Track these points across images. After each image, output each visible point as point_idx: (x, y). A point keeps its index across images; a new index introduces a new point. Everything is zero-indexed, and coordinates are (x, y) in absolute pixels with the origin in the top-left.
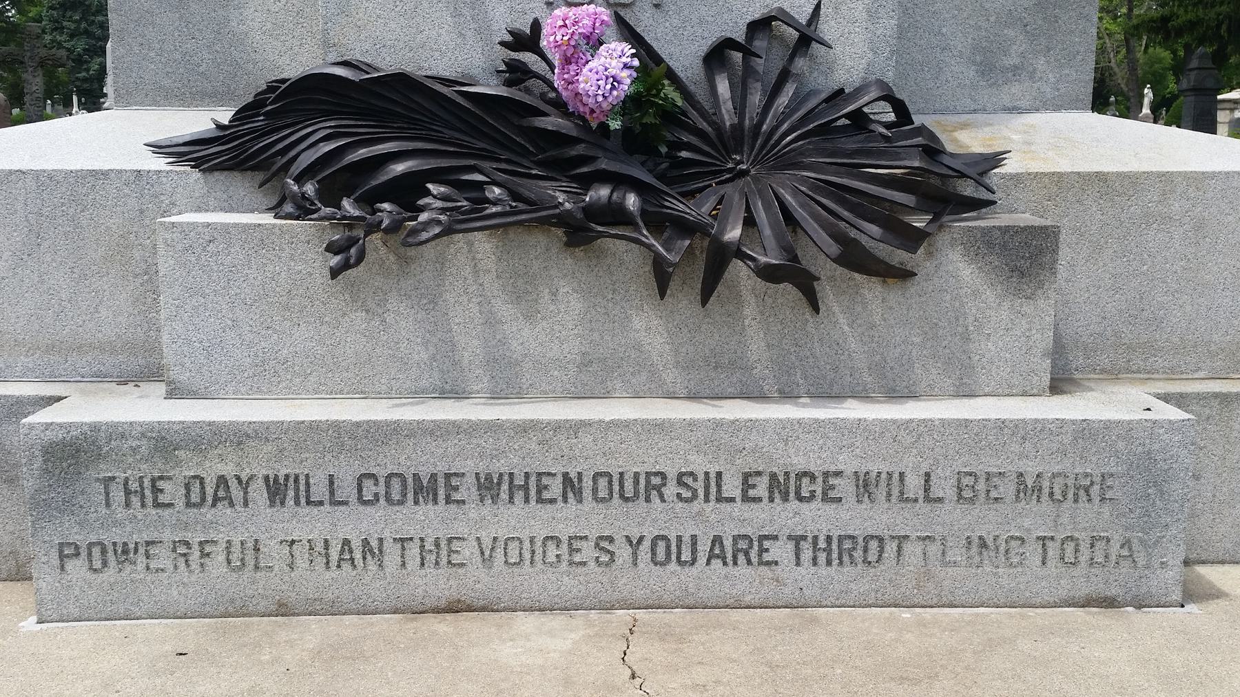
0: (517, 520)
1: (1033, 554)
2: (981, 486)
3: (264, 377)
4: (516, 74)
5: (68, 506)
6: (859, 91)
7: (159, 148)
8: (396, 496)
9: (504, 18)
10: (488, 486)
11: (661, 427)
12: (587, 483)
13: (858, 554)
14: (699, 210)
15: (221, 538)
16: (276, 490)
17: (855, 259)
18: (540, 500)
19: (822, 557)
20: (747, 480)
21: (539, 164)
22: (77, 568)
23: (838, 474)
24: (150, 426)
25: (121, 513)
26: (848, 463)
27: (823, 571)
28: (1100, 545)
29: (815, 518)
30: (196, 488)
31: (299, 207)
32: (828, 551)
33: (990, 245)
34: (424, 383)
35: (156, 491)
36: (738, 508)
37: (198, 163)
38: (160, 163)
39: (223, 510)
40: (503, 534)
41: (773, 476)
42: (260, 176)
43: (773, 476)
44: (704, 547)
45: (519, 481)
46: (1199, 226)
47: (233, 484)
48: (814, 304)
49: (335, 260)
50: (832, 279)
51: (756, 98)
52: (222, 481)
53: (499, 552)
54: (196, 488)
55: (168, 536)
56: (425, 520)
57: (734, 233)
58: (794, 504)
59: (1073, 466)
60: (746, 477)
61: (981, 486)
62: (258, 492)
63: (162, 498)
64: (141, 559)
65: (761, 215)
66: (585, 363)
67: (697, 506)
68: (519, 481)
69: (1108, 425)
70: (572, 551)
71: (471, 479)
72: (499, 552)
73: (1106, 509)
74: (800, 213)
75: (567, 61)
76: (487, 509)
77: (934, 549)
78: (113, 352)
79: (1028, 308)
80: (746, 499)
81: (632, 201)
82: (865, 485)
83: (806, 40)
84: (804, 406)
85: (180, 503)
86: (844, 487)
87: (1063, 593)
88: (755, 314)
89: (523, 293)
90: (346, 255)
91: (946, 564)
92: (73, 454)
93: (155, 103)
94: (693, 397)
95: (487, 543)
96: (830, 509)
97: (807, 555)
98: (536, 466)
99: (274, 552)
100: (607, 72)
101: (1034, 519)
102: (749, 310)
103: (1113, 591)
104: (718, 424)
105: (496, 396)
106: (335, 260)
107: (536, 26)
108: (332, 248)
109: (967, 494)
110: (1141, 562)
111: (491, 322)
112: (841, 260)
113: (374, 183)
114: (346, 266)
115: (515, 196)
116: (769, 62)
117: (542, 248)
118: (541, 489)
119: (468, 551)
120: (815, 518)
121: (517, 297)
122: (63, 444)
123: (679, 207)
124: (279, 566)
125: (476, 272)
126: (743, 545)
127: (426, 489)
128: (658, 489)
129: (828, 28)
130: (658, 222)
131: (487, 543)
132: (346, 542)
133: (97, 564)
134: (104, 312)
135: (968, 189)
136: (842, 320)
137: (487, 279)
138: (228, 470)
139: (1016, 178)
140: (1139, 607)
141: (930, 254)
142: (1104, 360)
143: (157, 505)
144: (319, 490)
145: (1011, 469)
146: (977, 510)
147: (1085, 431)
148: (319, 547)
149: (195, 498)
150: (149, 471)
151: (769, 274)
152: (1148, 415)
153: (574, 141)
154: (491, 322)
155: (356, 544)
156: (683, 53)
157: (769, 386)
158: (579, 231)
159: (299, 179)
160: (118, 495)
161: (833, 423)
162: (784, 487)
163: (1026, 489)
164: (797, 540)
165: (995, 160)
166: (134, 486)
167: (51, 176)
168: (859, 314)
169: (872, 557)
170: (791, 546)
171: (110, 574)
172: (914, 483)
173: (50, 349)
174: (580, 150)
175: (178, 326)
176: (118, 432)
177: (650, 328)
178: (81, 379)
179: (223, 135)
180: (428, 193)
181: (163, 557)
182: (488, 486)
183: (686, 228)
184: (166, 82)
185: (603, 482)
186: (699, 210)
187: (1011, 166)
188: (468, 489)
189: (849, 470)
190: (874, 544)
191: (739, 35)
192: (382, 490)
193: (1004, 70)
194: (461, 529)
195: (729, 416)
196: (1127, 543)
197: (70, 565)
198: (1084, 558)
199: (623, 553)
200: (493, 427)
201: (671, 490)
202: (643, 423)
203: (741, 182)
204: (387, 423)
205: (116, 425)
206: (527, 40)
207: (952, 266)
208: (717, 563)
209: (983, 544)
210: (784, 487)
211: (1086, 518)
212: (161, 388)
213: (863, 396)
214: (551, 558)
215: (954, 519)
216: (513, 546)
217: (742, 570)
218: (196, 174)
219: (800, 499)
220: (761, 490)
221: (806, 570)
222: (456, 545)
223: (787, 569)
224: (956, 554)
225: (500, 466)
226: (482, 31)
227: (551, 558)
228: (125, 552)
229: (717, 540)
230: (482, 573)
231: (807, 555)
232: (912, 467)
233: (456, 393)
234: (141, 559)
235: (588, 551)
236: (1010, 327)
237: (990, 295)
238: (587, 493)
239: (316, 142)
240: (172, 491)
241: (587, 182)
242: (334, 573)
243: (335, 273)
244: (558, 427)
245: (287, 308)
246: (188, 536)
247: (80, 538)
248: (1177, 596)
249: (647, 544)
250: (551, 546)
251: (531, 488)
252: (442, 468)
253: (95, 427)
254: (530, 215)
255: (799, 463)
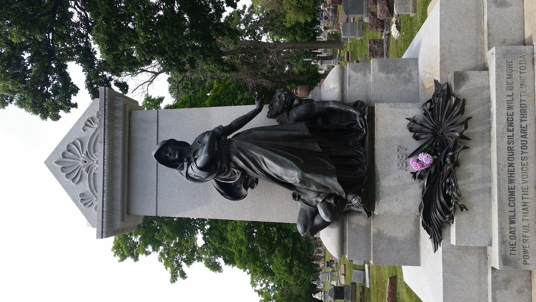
0: (518, 175)
1: (522, 75)
2: (510, 86)
3: (488, 227)
4: (421, 177)
5: (516, 262)
6: (424, 110)
7: (436, 250)
8: (513, 199)
9: (409, 179)
10: (511, 181)
11: (498, 147)
12: (510, 162)
13: (524, 109)
14: (452, 141)
15: (522, 233)
16: (512, 222)
17: (462, 111)
18: (514, 171)
19: (525, 116)
20: (509, 131)
21: (440, 172)
22: (528, 261)
23: (507, 113)
24: (499, 245)
25: (517, 252)
26: (505, 111)
27: (528, 115)
28: (521, 62)
29: (517, 117)
30: (512, 237)
31: (451, 219)
32: (523, 115)
33: (458, 84)
34: (488, 195)
35: (512, 245)
36: (515, 132)
37: (440, 241)
38: (440, 249)
39: (516, 232)
40: (521, 179)
41: (508, 126)
42: (443, 228)
43: (508, 126)
44: (523, 139)
45: (510, 175)
46: (451, 41)
47: (511, 230)
48: (470, 118)
49: (464, 210)
50: (467, 115)
51: (426, 130)
52: (510, 232)
53: (525, 179)
54: (512, 237)
55: (522, 243)
56: (518, 194)
57: (457, 134)
58: (514, 122)
59: (505, 69)
60: (508, 131)
61: (510, 86)
62: (513, 226)
63: (514, 244)
64: (527, 249)
65: (453, 129)
66: (483, 163)
67: (514, 140)
68: (510, 175)
69: (496, 62)
70: (524, 165)
71: (510, 185)
72: (525, 179)
73: (514, 62)
74: (453, 122)
75: (423, 166)
76: (516, 182)
77: (523, 94)
78: (481, 260)
79: (471, 76)
80: (513, 131)
81: (450, 154)
82: (510, 108)
83: (413, 121)
84: (492, 119)
85: (515, 241)
86: (510, 112)
87: (531, 69)
88: (474, 130)
89: (469, 175)
90: (463, 208)
91: (526, 92)
92: (505, 260)
93: (419, 257)
94: (490, 142)
95: (523, 182)
96: (515, 114)
97: (524, 119)
98: (507, 172)
99: (525, 223)
100: (425, 159)
101: (516, 75)
102: (472, 131)
103: (531, 59)
104: (497, 137)
105: (490, 181)
106: (464, 210)
107: (412, 173)
108: (462, 210)
109: (511, 88)
110: (525, 54)
111: (474, 182)
112: (463, 114)
113: (446, 204)
114: (465, 208)
115: (449, 176)
116: (417, 127)
117: (459, 172)
118: (511, 171)
119: (525, 186)
120: (517, 117)
121: (469, 176)
122: (503, 262)
123: (451, 145)
124: (528, 222)
125: (465, 184)
126: (523, 131)
127: (512, 193)
128: (511, 148)
129: (411, 116)
130: (454, 149)
131: (523, 182)
132: (523, 209)
133: (528, 257)
134: (472, 262)
135: (445, 87)
136: (473, 112)
137: (466, 183)
138: (508, 231)
139: (441, 78)
140: (534, 54)
141: (460, 96)
142: (479, 58)
143: (515, 245)
144: (512, 214)
145: (506, 80)
146: (515, 86)
147: (498, 66)
148: (524, 214)
149: (514, 238)
150: (508, 246)
151: (466, 127)
152: (494, 54)
153: (437, 165)
154: (474, 182)
155: (523, 207)
156: (415, 145)
157: (488, 126)
158: (456, 164)
159: (445, 218)
160: (513, 252)
161: (497, 114)
162: (510, 123)
163: (510, 76)
164: (521, 121)
165: (436, 82)
166: (511, 249)
167: (444, 270)
168: (473, 109)
169: (525, 106)
170: (523, 122)
171: (529, 255)
172: (509, 98)
173: (480, 273)
174: (438, 164)
175: (477, 243)
176: (500, 251)
177: (475, 150)
178: (486, 264)
179: (433, 237)
180: (448, 193)
181: (526, 245)
182: (511, 181)
183: (456, 143)
184: (415, 255)
185: (510, 159)
186: (452, 141)
187: (438, 79)
188: (512, 185)
189: (506, 111)
190: (522, 106)
191: (413, 134)
192: (512, 202)
193: (409, 77)
194: (520, 187)
195: (496, 135)
196: (521, 57)
197: (528, 262)
198: (524, 65)
199: (525, 155)
200: (499, 180)
201: (511, 146)
202: (497, 151)
203: (444, 133)
204: (498, 200)
205: (499, 252)
206: (414, 174)
207: (463, 91)
208: (527, 136)
209: (522, 84)
210: (510, 123)
211: (516, 66)
212: (489, 248)
213: (490, 107)
214: (526, 169)
215: (516, 91)
216: (523, 177)
217: (528, 131)
218: (443, 241)
219: (513, 120)
220: (511, 128)
221: (527, 119)
222: (523, 188)
223: (527, 123)
224: (524, 90)
225: (507, 179)
226: (412, 184)
227: (526, 169)
228: (525, 252)
229: (522, 136)
230: (530, 183)
231: (524, 119)
232: (506, 99)
233: (490, 190)
234: (527, 249)
235: (525, 162)
236: (475, 79)
237: (468, 84)
238: (512, 162)
239: (436, 215)
240: (513, 242)
241: (445, 162)
242: (529, 212)
243: (467, 210)
244: (498, 168)
245: (472, 222)
246: (522, 239)
247: (522, 260)
248: (532, 46)
249: (523, 150)
250: (523, 169)
251: (511, 173)
252: (507, 190)
253: (500, 255)
254: (451, 174)
255: (505, 121)
